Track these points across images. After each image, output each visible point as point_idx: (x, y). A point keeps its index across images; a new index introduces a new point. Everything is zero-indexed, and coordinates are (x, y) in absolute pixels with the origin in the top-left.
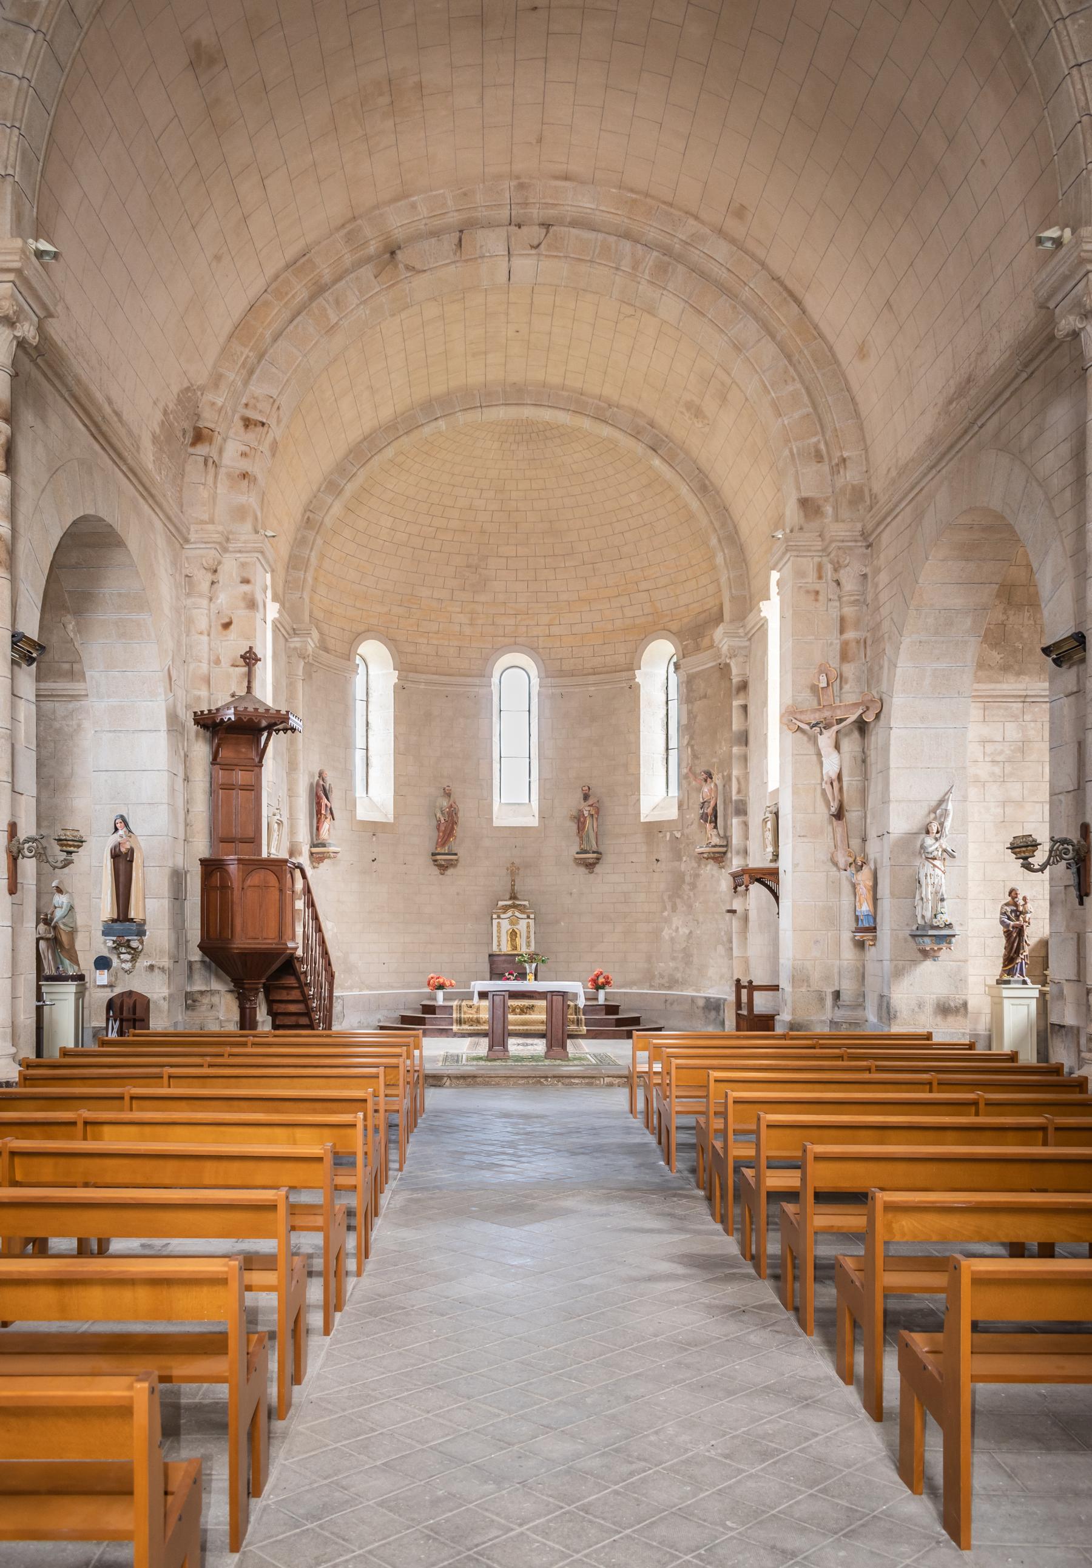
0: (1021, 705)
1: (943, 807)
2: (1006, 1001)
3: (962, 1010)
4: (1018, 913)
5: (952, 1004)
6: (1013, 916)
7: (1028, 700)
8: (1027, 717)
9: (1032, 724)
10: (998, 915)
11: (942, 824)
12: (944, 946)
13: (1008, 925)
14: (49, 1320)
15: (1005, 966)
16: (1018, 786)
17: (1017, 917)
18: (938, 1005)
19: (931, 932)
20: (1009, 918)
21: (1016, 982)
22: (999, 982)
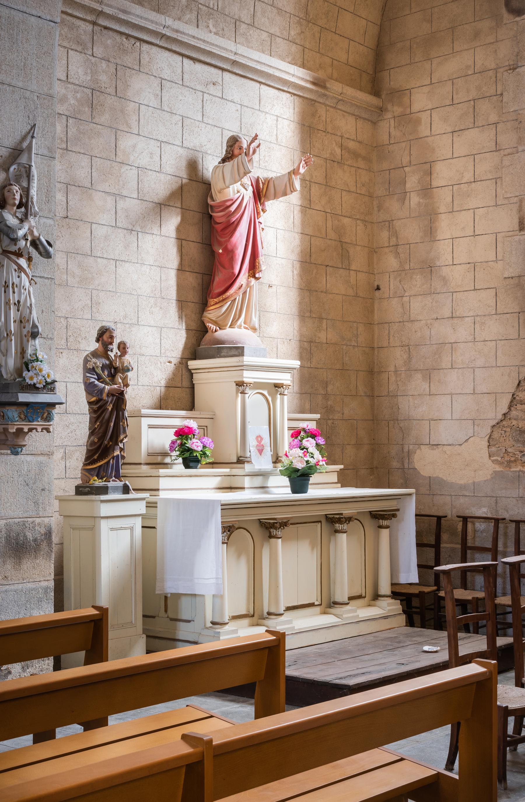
0: (90, 27)
1: (23, 159)
2: (104, 525)
3: (44, 545)
4: (115, 370)
5: (30, 536)
6: (105, 374)
7: (102, 22)
8: (99, 51)
9: (104, 64)
10: (79, 377)
11: (26, 191)
12: (39, 423)
13: (102, 390)
14: (37, 191)
15: (85, 465)
16: (85, 161)
17: (113, 376)
18: (8, 539)
19: (23, 397)
20: (99, 378)
21: (115, 489)
22: (80, 491)
